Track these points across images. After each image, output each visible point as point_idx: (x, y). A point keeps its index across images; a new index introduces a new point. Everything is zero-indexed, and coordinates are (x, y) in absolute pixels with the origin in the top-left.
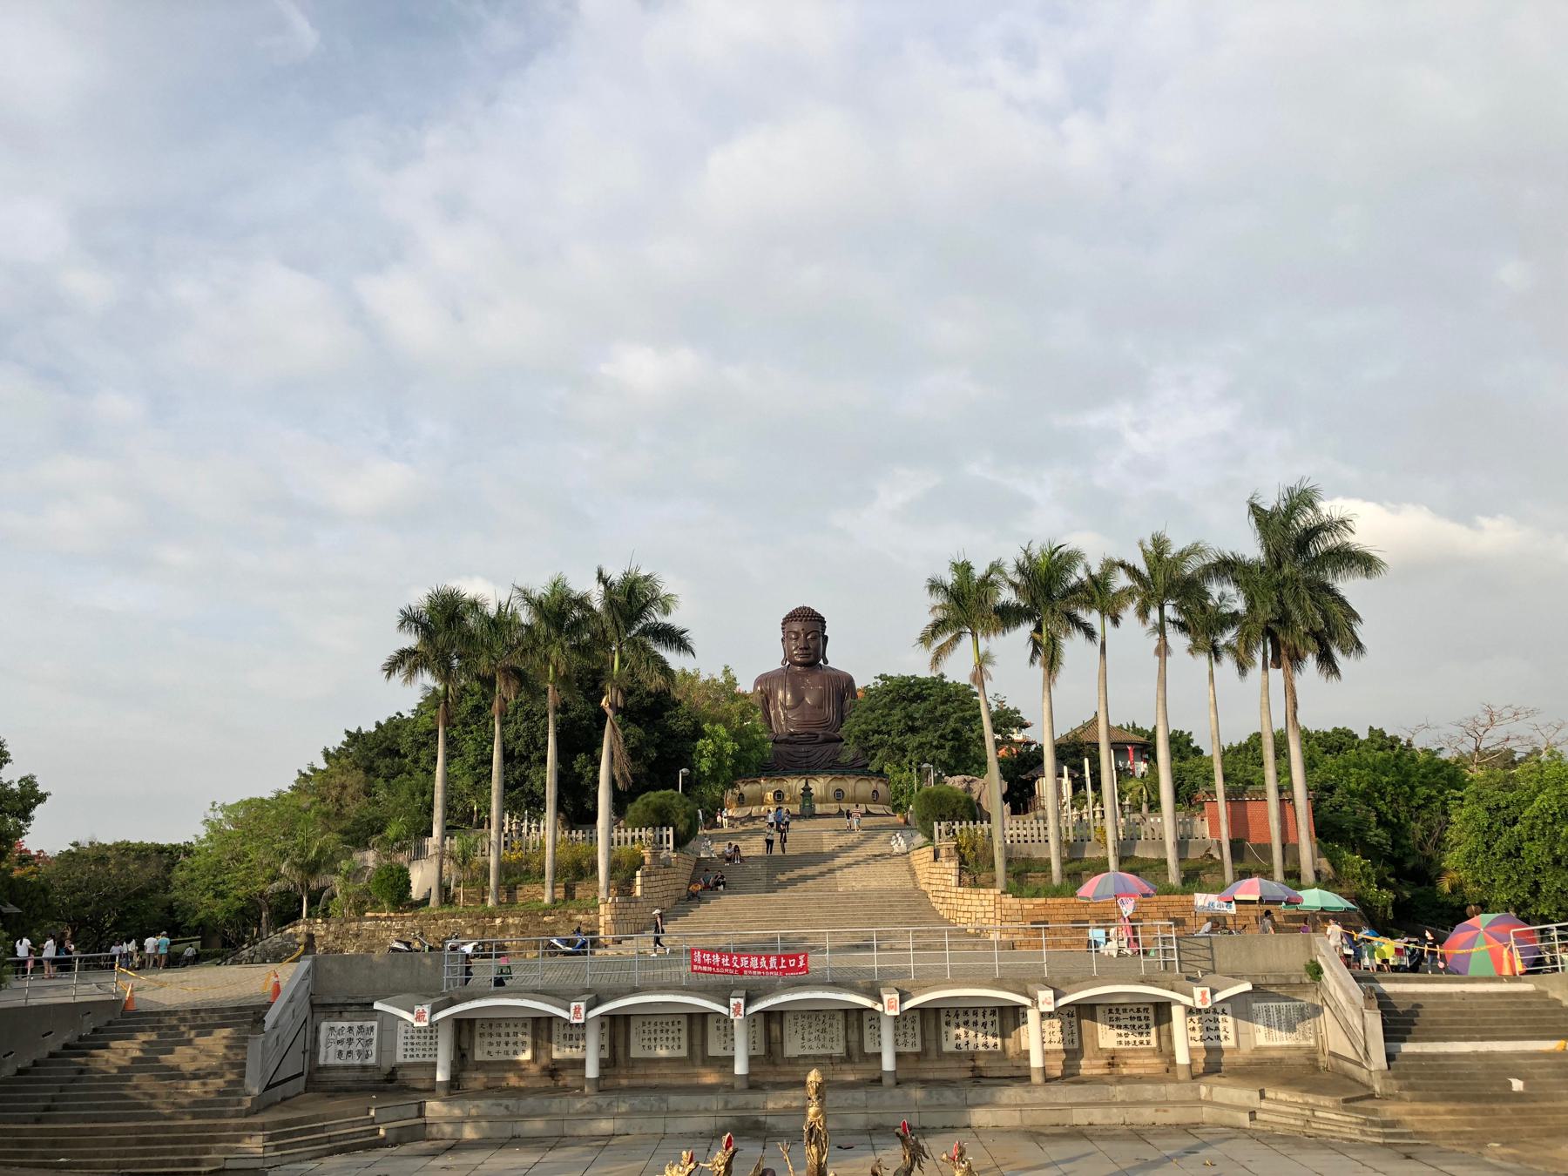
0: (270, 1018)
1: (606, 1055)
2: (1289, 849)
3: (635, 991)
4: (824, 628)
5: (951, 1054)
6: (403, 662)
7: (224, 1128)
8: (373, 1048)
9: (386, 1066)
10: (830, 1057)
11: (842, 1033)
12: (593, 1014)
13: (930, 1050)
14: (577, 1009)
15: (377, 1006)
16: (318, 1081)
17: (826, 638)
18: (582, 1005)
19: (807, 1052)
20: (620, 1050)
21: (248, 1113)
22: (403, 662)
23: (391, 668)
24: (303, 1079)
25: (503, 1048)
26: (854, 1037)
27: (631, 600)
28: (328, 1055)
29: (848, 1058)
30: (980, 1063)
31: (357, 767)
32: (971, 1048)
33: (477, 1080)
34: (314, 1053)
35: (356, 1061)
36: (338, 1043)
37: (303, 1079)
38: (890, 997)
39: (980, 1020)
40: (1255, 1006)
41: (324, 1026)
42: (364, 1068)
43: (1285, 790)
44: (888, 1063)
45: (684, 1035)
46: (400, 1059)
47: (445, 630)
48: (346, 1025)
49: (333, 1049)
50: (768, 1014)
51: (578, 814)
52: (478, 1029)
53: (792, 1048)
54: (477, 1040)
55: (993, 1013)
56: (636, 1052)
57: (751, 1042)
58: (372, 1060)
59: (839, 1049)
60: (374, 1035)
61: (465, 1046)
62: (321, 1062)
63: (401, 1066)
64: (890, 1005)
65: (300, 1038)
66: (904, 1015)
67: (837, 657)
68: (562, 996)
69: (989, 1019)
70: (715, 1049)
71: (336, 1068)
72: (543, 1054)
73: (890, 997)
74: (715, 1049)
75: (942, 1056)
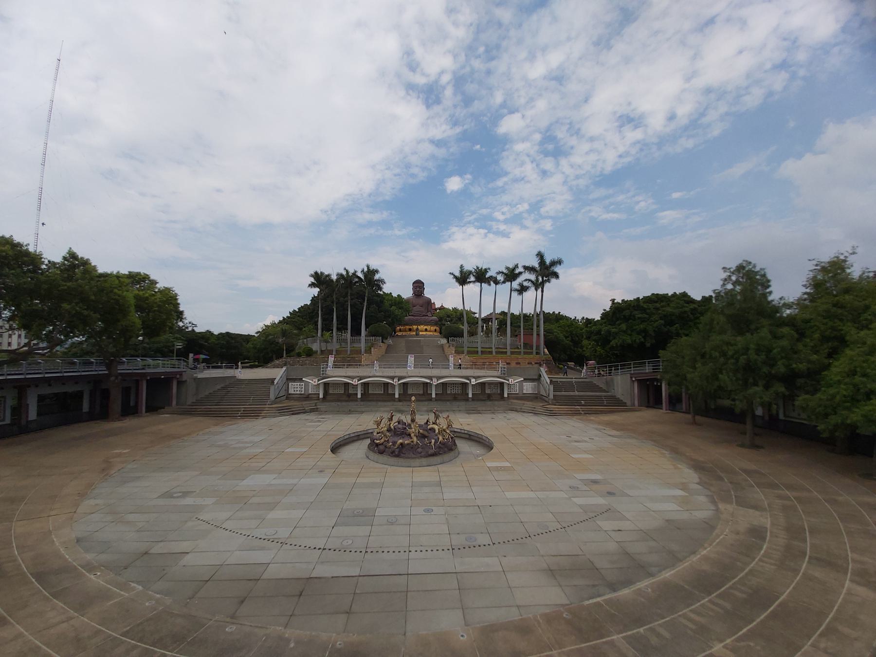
0: (276, 382)
2: (538, 347)
6: (312, 285)
16: (289, 397)
22: (312, 285)
23: (310, 285)
27: (370, 273)
28: (291, 391)
29: (423, 394)
33: (328, 397)
36: (295, 388)
38: (435, 380)
43: (538, 335)
44: (470, 396)
47: (320, 280)
50: (404, 383)
51: (356, 332)
53: (410, 392)
57: (399, 390)
59: (421, 392)
64: (435, 382)
67: (427, 293)
68: (352, 378)
70: (390, 392)
74: (390, 392)
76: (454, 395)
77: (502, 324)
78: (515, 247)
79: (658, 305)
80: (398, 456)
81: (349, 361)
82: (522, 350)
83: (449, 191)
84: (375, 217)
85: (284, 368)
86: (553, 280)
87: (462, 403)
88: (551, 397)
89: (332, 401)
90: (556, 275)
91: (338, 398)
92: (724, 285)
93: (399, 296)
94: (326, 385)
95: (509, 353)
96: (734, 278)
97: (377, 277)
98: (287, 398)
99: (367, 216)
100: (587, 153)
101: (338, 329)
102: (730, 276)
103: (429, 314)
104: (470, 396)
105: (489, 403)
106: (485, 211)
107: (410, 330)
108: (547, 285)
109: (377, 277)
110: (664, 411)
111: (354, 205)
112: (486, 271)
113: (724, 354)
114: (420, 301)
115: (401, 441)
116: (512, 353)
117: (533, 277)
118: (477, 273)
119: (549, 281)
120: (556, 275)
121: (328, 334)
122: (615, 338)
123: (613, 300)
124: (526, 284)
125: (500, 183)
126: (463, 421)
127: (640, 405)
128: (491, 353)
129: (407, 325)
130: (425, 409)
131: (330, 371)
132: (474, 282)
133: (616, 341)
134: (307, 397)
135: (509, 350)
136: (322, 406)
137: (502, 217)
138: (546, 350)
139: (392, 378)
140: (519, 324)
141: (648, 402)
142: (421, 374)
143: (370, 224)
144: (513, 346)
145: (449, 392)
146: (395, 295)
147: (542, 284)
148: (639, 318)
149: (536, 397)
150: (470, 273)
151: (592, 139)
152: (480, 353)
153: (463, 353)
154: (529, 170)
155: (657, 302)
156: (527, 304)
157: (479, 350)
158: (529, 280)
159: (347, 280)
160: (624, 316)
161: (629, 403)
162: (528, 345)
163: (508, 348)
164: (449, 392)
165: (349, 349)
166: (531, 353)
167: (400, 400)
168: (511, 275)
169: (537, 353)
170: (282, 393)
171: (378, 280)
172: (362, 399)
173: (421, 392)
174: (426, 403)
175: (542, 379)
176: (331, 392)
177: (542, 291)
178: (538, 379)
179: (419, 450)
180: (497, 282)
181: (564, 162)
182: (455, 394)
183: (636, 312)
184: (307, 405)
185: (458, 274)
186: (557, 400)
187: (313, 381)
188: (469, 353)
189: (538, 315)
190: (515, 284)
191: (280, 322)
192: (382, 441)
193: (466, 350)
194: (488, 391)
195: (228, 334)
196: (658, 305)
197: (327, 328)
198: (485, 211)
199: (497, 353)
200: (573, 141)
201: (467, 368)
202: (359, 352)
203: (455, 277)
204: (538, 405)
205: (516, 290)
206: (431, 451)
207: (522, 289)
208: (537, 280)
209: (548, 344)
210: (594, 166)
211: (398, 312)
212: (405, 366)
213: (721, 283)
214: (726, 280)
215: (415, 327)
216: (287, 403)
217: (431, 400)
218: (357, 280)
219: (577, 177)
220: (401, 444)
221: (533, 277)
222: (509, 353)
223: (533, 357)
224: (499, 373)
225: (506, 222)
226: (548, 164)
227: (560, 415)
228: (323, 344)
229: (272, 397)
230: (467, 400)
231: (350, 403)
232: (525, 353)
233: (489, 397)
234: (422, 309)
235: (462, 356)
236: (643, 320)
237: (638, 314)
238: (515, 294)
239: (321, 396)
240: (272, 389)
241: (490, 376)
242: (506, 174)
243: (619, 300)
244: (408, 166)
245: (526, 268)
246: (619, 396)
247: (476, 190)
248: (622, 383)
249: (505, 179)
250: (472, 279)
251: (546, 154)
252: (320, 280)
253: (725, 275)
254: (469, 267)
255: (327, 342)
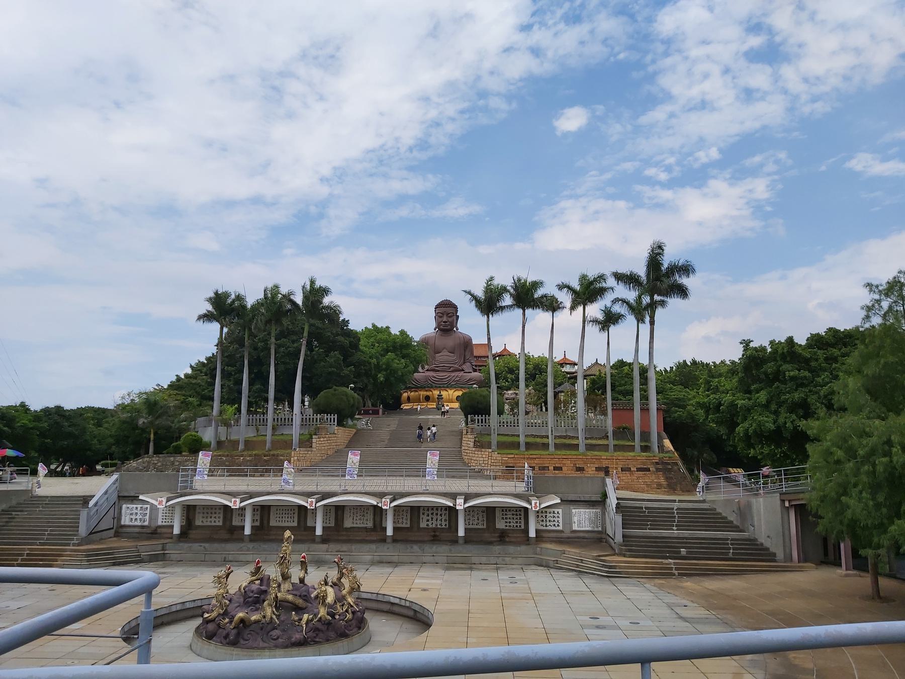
0: (91, 503)
1: (258, 524)
2: (646, 436)
3: (269, 494)
4: (457, 311)
5: (424, 528)
7: (65, 550)
8: (147, 517)
9: (153, 525)
10: (366, 528)
11: (372, 516)
12: (318, 504)
13: (339, 520)
14: (235, 502)
15: (141, 497)
16: (119, 531)
17: (458, 317)
18: (314, 500)
19: (355, 525)
20: (265, 522)
21: (79, 545)
24: (113, 531)
25: (213, 519)
26: (378, 519)
28: (125, 520)
30: (437, 534)
31: (668, 42)
32: (434, 526)
33: (193, 534)
34: (119, 519)
35: (138, 523)
36: (131, 515)
37: (113, 531)
39: (439, 513)
40: (573, 511)
41: (124, 506)
42: (143, 527)
44: (390, 532)
45: (296, 516)
46: (160, 523)
47: (223, 308)
48: (135, 506)
49: (128, 518)
52: (198, 511)
53: (348, 523)
54: (197, 515)
55: (446, 510)
56: (273, 523)
58: (146, 523)
59: (370, 525)
60: (148, 512)
61: (191, 518)
62: (123, 523)
63: (160, 527)
65: (112, 510)
66: (465, 509)
68: (309, 495)
69: (444, 512)
70: (309, 524)
71: (129, 526)
72: (228, 523)
73: (460, 501)
75: (420, 529)
76: (348, 529)
77: (596, 385)
78: (615, 243)
79: (835, 352)
80: (234, 644)
81: (267, 463)
82: (611, 442)
83: (558, 133)
84: (414, 185)
85: (115, 476)
86: (674, 302)
87: (444, 549)
88: (619, 538)
89: (196, 541)
90: (682, 291)
91: (212, 536)
92: (868, 317)
93: (403, 332)
94: (190, 510)
95: (582, 448)
96: (885, 304)
97: (326, 301)
98: (117, 534)
99: (397, 186)
100: (834, 53)
101: (277, 400)
102: (878, 301)
103: (467, 367)
104: (390, 532)
105: (497, 548)
106: (629, 166)
107: (427, 399)
108: (659, 312)
109: (326, 301)
110: (841, 571)
111: (380, 161)
112: (536, 285)
113: (851, 453)
114: (449, 341)
115: (241, 615)
116: (590, 447)
117: (631, 295)
118: (516, 288)
119: (663, 303)
120: (682, 291)
121: (231, 409)
122: (745, 419)
123: (746, 343)
124: (618, 308)
125: (658, 114)
126: (376, 580)
127: (805, 558)
128: (545, 446)
129: (422, 388)
130: (368, 558)
131: (202, 481)
132: (510, 307)
133: (746, 424)
134: (153, 533)
135: (581, 442)
136: (173, 551)
137: (663, 176)
138: (667, 443)
139: (381, 495)
140: (615, 385)
141: (826, 553)
142: (368, 489)
143: (402, 199)
144: (590, 431)
145: (423, 525)
146: (395, 331)
147: (652, 306)
148: (792, 378)
149: (597, 539)
150: (504, 289)
151: (843, 27)
152: (523, 448)
153: (489, 446)
154: (714, 86)
155: (833, 346)
156: (623, 343)
157: (522, 439)
158: (624, 301)
159: (275, 306)
160: (766, 374)
161: (780, 555)
162: (623, 431)
163: (581, 435)
164: (423, 525)
165: (269, 438)
166: (632, 448)
167: (324, 540)
168: (588, 291)
169: (646, 449)
170: (107, 523)
171: (581, 285)
172: (253, 538)
173: (370, 525)
174: (373, 546)
175: (608, 501)
176: (198, 522)
177: (652, 323)
178: (601, 501)
179: (275, 633)
180: (552, 305)
181: (788, 72)
182: (435, 530)
183: (785, 367)
184: (147, 547)
185: (480, 293)
186: (630, 546)
187: (158, 501)
188: (501, 446)
189: (644, 371)
190: (595, 310)
191: (172, 386)
192: (214, 614)
193: (494, 439)
194: (500, 525)
195: (59, 410)
196: (835, 352)
197: (232, 397)
198: (629, 166)
199: (557, 446)
200: (807, 33)
201: (495, 478)
202: (288, 445)
203: (474, 298)
204: (589, 556)
205: (595, 321)
206: (297, 636)
207: (610, 319)
208: (639, 299)
209: (672, 429)
210: (846, 78)
211: (399, 364)
212: (419, 471)
213: (863, 313)
214: (869, 309)
215: (436, 393)
216: (115, 543)
217: (384, 540)
218: (289, 306)
219: (815, 99)
220: (242, 621)
221: (631, 295)
222: (582, 448)
223: (637, 456)
224: (521, 487)
225: (669, 185)
226: (759, 77)
227: (628, 575)
228: (222, 430)
229: (83, 530)
230: (455, 541)
231: (229, 546)
232: (617, 448)
233: (503, 537)
234: (452, 357)
235: (486, 452)
236: (800, 384)
237: (790, 371)
238: (593, 330)
239: (176, 531)
240: (84, 514)
241: (499, 492)
242: (668, 97)
243: (761, 341)
244: (483, 94)
245: (619, 277)
246: (762, 539)
247: (615, 130)
248: (762, 509)
249: (669, 108)
250: (507, 300)
251: (754, 56)
252: (223, 308)
253: (867, 298)
254: (505, 279)
255: (227, 424)
